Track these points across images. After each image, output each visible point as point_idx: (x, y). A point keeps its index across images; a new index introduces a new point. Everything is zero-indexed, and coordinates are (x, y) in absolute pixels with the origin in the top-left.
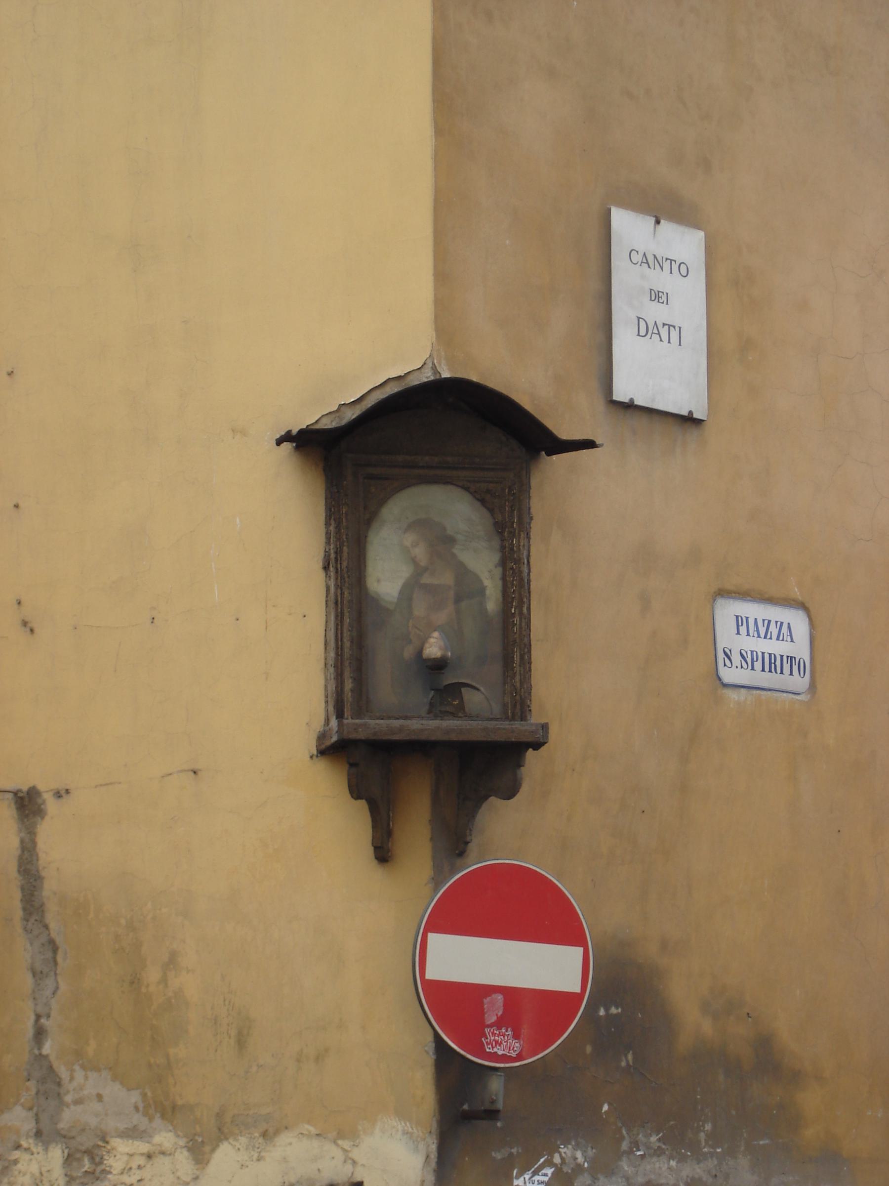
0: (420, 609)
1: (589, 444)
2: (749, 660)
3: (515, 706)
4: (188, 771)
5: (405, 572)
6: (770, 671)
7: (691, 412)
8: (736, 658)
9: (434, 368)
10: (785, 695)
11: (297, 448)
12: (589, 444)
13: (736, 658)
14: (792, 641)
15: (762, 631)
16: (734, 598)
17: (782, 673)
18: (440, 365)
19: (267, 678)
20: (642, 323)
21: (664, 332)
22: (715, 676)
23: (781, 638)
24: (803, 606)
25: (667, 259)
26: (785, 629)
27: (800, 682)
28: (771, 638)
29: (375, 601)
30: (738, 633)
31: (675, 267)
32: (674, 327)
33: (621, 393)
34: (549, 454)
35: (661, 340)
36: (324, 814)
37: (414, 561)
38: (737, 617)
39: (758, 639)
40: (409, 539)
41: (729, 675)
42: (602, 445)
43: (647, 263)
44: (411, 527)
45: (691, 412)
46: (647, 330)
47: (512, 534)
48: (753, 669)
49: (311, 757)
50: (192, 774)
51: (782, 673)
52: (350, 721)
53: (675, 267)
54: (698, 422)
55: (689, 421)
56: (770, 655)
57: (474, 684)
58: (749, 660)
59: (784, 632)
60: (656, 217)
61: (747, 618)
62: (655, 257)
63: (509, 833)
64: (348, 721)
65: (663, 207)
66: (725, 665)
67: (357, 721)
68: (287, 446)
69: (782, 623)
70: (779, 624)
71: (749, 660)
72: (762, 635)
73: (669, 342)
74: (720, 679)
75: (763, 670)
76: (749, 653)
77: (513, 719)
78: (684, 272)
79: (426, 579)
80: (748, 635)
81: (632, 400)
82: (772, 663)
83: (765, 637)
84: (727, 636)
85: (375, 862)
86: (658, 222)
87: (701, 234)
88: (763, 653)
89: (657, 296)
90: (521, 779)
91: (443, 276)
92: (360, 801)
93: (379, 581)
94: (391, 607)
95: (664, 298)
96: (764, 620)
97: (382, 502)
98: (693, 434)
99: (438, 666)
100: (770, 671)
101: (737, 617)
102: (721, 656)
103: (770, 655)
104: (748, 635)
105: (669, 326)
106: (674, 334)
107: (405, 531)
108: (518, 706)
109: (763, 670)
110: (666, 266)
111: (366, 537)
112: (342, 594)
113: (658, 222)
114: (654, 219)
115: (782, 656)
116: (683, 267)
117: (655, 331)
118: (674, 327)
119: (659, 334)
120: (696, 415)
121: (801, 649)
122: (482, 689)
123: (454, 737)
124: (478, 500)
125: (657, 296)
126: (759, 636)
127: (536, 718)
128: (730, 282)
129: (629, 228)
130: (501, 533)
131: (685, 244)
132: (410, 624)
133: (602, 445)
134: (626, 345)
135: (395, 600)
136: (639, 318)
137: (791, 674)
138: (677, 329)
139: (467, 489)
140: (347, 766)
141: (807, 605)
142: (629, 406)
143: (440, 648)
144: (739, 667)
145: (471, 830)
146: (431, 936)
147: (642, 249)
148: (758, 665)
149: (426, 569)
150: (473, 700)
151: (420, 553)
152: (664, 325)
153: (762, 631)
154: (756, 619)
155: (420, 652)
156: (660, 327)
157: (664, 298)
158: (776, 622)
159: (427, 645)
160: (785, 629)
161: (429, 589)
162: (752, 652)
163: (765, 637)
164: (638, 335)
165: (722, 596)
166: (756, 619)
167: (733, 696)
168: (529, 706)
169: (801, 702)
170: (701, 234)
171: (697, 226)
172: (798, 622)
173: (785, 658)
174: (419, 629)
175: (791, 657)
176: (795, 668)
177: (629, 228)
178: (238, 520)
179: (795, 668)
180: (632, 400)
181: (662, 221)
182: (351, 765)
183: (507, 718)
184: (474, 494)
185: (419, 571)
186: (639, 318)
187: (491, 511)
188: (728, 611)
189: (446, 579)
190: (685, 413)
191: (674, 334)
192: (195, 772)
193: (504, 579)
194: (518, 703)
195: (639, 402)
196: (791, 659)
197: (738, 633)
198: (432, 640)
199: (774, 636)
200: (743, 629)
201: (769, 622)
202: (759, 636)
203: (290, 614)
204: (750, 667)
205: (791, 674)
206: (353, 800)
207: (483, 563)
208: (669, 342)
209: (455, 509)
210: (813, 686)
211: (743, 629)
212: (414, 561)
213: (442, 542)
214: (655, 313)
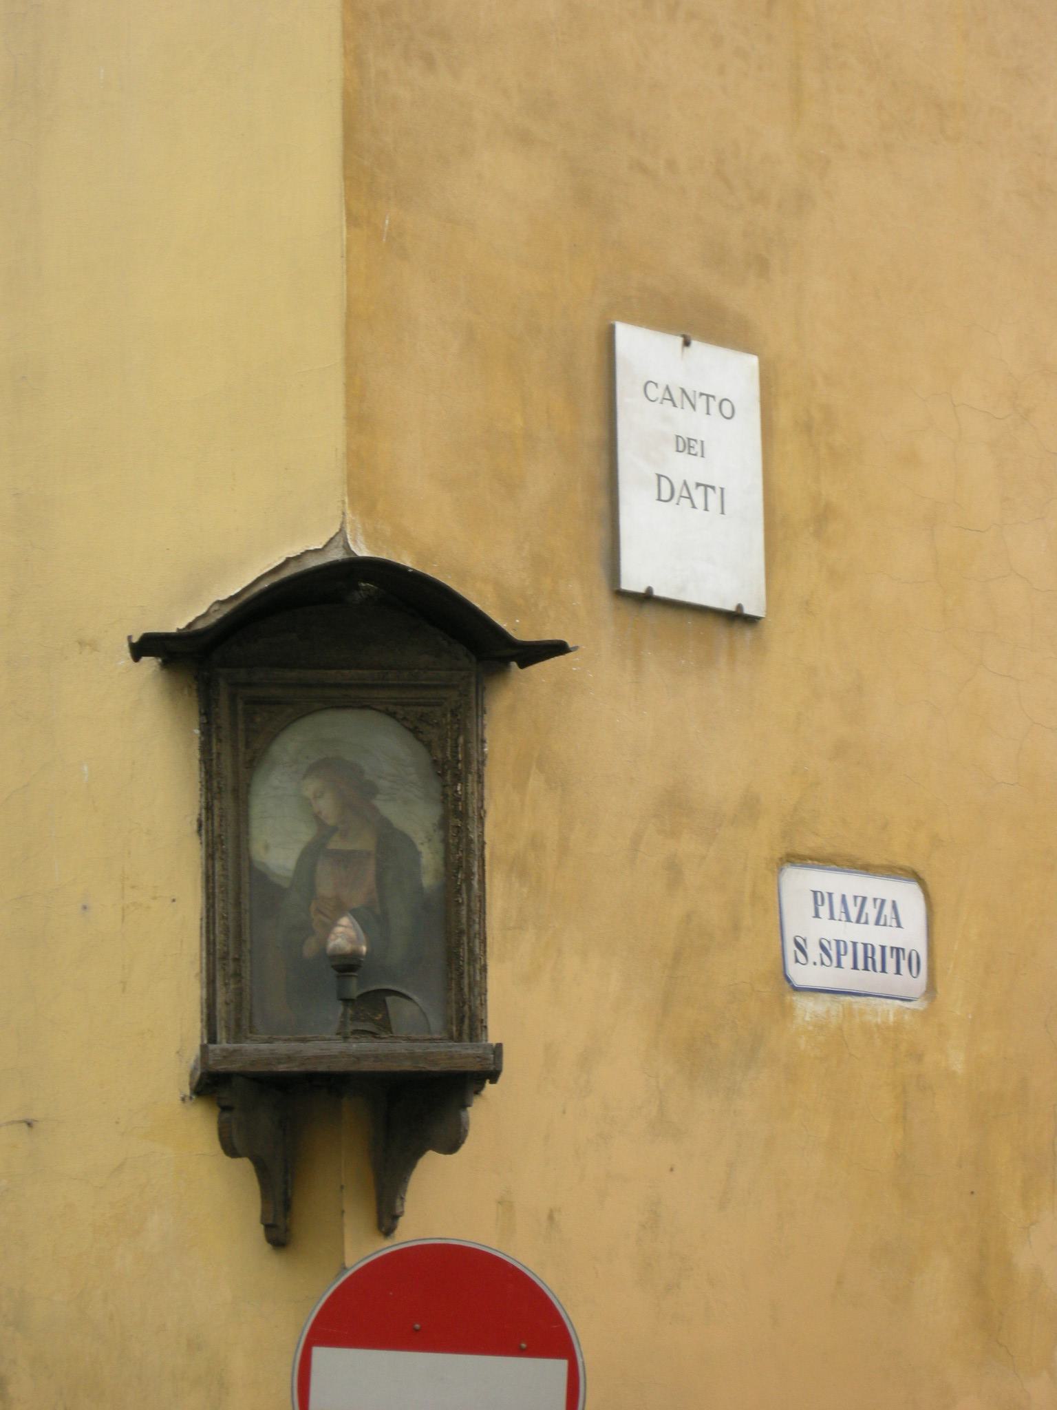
0: (326, 887)
1: (558, 648)
2: (833, 953)
3: (461, 1021)
4: (20, 1122)
5: (306, 834)
6: (866, 969)
7: (740, 607)
8: (814, 952)
9: (347, 547)
10: (889, 1001)
11: (165, 664)
12: (558, 648)
13: (814, 952)
14: (899, 926)
15: (854, 912)
16: (807, 866)
17: (883, 970)
18: (355, 541)
19: (124, 990)
20: (664, 482)
21: (698, 495)
22: (781, 977)
23: (882, 922)
24: (914, 876)
25: (702, 394)
26: (888, 910)
27: (914, 984)
28: (866, 923)
29: (261, 878)
30: (817, 916)
31: (714, 405)
32: (713, 488)
33: (632, 581)
34: (524, 664)
35: (694, 507)
36: (199, 1184)
37: (317, 817)
38: (815, 893)
39: (843, 925)
40: (311, 787)
41: (802, 974)
42: (576, 648)
43: (672, 400)
44: (314, 769)
45: (740, 607)
46: (669, 492)
47: (458, 777)
48: (839, 965)
49: (183, 1099)
50: (25, 1126)
51: (883, 970)
52: (225, 1045)
53: (714, 405)
54: (751, 620)
55: (737, 618)
56: (865, 945)
57: (404, 991)
58: (832, 952)
59: (889, 914)
60: (684, 336)
61: (830, 895)
62: (683, 391)
63: (446, 1201)
64: (223, 1044)
65: (695, 321)
66: (797, 961)
67: (236, 1046)
68: (150, 664)
69: (883, 901)
70: (878, 902)
71: (833, 953)
72: (854, 916)
73: (706, 509)
74: (788, 980)
75: (855, 967)
76: (834, 944)
77: (460, 1039)
78: (727, 412)
79: (336, 844)
80: (832, 918)
81: (649, 590)
82: (868, 958)
83: (858, 921)
84: (800, 921)
85: (267, 1247)
86: (687, 343)
87: (753, 360)
88: (855, 944)
89: (686, 445)
90: (467, 1123)
91: (360, 418)
92: (239, 1160)
93: (267, 847)
94: (286, 885)
95: (697, 449)
96: (855, 897)
97: (273, 737)
98: (747, 635)
99: (347, 966)
100: (866, 969)
101: (815, 893)
102: (790, 948)
103: (865, 945)
104: (832, 918)
105: (706, 486)
106: (714, 498)
107: (305, 777)
108: (467, 1022)
109: (855, 967)
110: (701, 403)
111: (249, 785)
112: (213, 866)
113: (687, 343)
114: (680, 340)
115: (883, 948)
116: (726, 405)
117: (685, 494)
118: (713, 488)
119: (690, 498)
120: (748, 610)
121: (912, 936)
122: (415, 998)
123: (367, 1066)
124: (410, 730)
125: (686, 445)
126: (848, 920)
127: (493, 1037)
128: (794, 426)
129: (642, 351)
130: (442, 775)
131: (732, 373)
132: (313, 907)
133: (576, 648)
134: (639, 512)
135: (290, 874)
136: (659, 476)
137: (898, 972)
138: (718, 491)
139: (392, 715)
140: (217, 1110)
141: (922, 876)
142: (647, 598)
143: (351, 941)
144: (819, 962)
145: (402, 1199)
146: (321, 1354)
147: (663, 381)
148: (847, 961)
149: (334, 830)
150: (402, 1013)
151: (327, 806)
152: (698, 485)
153: (854, 912)
154: (844, 897)
155: (325, 949)
156: (692, 486)
157: (697, 449)
158: (875, 900)
159: (332, 936)
160: (888, 910)
161: (344, 859)
162: (838, 942)
163: (858, 921)
164: (659, 499)
165: (793, 864)
166: (844, 897)
167: (808, 1007)
168: (482, 1021)
169: (914, 1012)
170: (753, 360)
171: (748, 349)
172: (908, 897)
173: (888, 951)
174: (325, 915)
175: (898, 949)
176: (878, 957)
177: (642, 351)
178: (86, 768)
179: (878, 957)
180: (649, 590)
181: (694, 343)
182: (224, 1109)
183: (451, 1038)
184: (402, 720)
185: (325, 831)
186: (659, 476)
187: (428, 745)
188: (800, 883)
189: (364, 842)
190: (731, 607)
191: (714, 498)
192: (29, 1124)
193: (445, 841)
194: (466, 1016)
195: (657, 592)
196: (898, 951)
197: (817, 916)
198: (339, 929)
199: (872, 919)
200: (825, 911)
201: (864, 899)
202: (848, 920)
203: (155, 898)
204: (835, 963)
205: (898, 972)
206: (228, 1159)
207: (417, 820)
208: (706, 509)
209: (381, 748)
210: (931, 988)
211: (825, 911)
212: (317, 817)
213: (358, 793)
214: (683, 468)
